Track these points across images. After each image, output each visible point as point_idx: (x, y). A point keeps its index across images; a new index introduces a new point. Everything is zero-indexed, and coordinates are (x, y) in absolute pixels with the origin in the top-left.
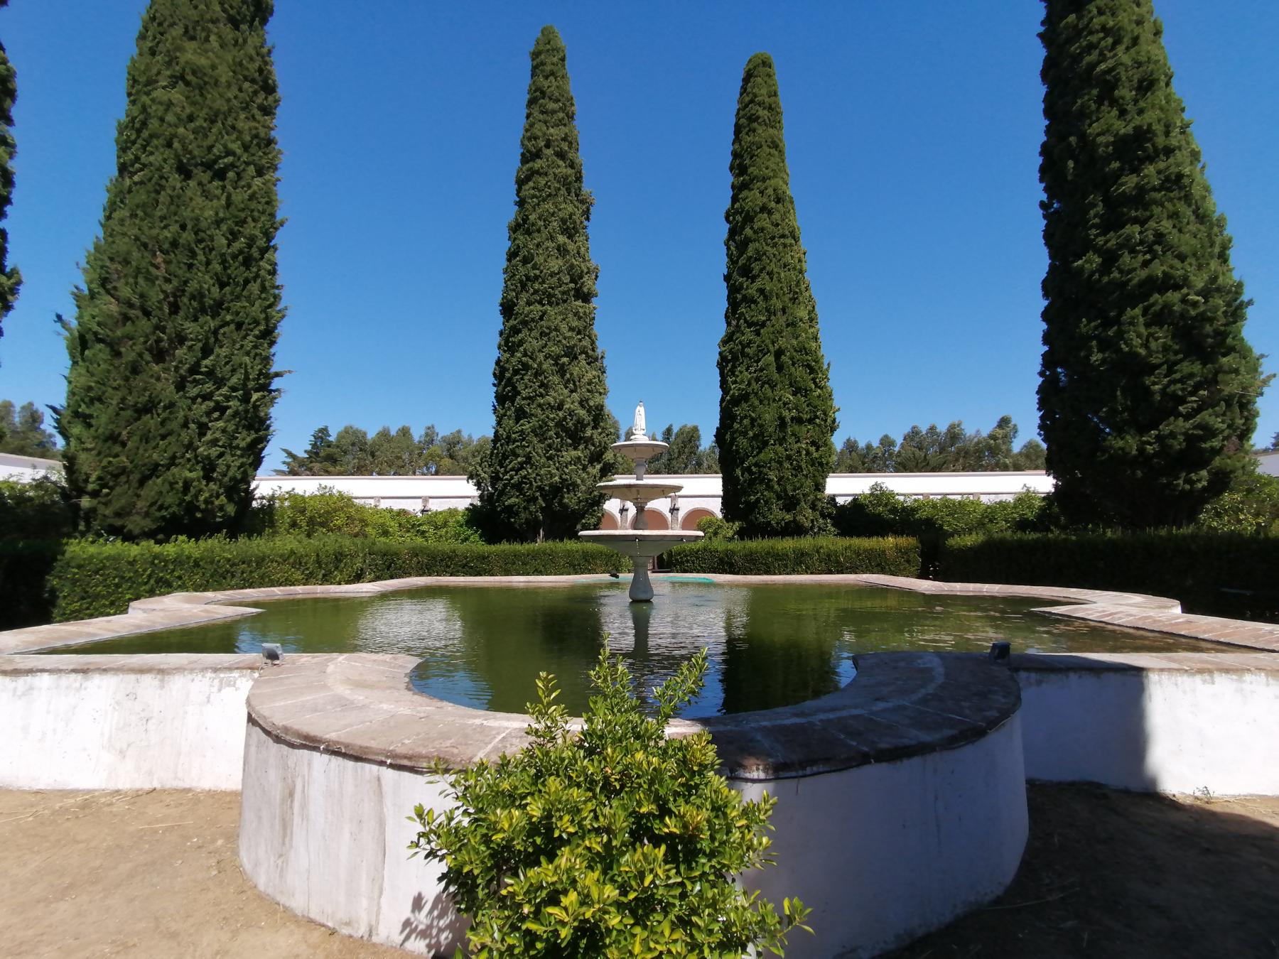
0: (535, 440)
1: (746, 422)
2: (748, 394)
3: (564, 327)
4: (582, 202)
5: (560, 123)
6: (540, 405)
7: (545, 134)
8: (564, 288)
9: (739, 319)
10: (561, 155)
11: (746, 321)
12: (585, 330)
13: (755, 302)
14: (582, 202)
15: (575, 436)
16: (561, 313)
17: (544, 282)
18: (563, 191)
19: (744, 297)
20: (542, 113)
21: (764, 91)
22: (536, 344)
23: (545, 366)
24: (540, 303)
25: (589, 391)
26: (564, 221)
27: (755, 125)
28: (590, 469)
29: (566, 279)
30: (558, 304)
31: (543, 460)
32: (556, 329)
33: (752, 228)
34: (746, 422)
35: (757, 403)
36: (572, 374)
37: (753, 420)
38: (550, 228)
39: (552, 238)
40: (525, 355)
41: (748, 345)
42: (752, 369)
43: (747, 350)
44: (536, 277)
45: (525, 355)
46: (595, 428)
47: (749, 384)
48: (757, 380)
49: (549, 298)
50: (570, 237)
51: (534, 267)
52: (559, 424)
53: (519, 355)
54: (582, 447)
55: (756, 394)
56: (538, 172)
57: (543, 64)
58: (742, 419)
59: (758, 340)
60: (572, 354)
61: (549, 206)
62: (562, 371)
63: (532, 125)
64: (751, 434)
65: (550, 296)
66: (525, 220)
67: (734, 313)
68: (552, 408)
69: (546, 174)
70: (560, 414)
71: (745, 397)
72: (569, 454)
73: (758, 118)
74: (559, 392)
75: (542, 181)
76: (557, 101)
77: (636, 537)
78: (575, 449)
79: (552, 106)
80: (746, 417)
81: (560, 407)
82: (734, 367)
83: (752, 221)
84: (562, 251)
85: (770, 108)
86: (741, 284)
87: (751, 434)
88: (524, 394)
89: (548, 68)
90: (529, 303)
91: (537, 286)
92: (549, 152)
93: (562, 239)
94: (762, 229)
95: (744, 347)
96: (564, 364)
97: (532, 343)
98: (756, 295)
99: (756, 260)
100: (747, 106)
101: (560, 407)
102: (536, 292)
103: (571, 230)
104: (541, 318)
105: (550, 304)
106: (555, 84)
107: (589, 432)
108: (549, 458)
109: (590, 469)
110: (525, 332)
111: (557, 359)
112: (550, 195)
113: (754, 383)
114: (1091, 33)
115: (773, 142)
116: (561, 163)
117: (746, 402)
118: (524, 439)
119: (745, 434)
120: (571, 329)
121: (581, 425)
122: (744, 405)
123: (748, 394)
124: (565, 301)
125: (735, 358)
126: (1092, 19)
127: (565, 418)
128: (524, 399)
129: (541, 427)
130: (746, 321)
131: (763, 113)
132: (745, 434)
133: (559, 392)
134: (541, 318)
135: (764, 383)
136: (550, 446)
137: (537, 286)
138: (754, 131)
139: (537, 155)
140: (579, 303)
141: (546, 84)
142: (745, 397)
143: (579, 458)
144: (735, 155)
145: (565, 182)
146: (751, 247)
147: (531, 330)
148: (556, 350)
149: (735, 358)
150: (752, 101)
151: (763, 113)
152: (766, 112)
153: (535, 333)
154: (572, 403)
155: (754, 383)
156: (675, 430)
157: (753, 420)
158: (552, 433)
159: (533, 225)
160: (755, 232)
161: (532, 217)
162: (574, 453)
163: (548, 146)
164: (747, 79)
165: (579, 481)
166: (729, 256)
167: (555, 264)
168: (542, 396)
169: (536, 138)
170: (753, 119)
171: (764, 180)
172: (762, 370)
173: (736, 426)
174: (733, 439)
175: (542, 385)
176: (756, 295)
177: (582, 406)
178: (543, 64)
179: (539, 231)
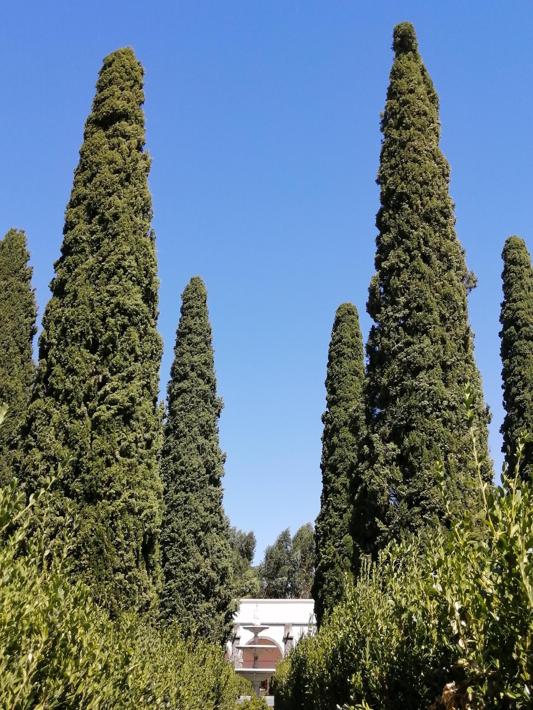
0: (179, 595)
1: (332, 584)
2: (333, 563)
3: (201, 509)
4: (216, 407)
5: (203, 351)
6: (183, 569)
7: (190, 362)
8: (202, 479)
9: (328, 505)
10: (202, 375)
11: (333, 507)
12: (215, 510)
13: (339, 493)
14: (216, 407)
15: (207, 592)
16: (199, 497)
17: (188, 476)
18: (203, 403)
19: (332, 488)
20: (189, 344)
21: (348, 334)
22: (181, 523)
23: (187, 540)
24: (184, 490)
25: (218, 557)
26: (202, 426)
27: (342, 359)
28: (217, 616)
29: (203, 471)
30: (197, 491)
31: (185, 610)
32: (196, 511)
33: (338, 437)
34: (332, 584)
35: (339, 570)
36: (205, 544)
37: (337, 583)
38: (192, 432)
39: (194, 440)
40: (173, 531)
41: (334, 526)
42: (337, 544)
43: (334, 529)
44: (183, 472)
45: (173, 531)
46: (221, 584)
47: (334, 556)
48: (340, 552)
49: (190, 487)
50: (206, 438)
51: (182, 464)
52: (197, 582)
53: (168, 531)
54: (212, 600)
55: (339, 563)
56: (185, 391)
57: (191, 307)
58: (329, 582)
59: (341, 522)
60: (205, 528)
61: (193, 416)
62: (198, 542)
63: (182, 354)
64: (335, 593)
65: (192, 486)
66: (176, 427)
67: (326, 499)
68: (191, 571)
69: (191, 391)
70: (197, 575)
71: (330, 566)
72: (203, 606)
73: (344, 354)
74: (197, 558)
75: (188, 397)
76: (200, 334)
77: (254, 672)
78: (207, 601)
79: (197, 339)
80: (332, 580)
81: (197, 570)
82: (324, 541)
83: (338, 431)
84: (201, 449)
85: (353, 346)
86: (331, 478)
87: (335, 593)
88: (172, 560)
89: (195, 310)
90: (177, 491)
91: (183, 478)
92: (193, 374)
93: (201, 440)
94: (345, 439)
95: (331, 527)
96: (200, 537)
97: (178, 522)
98: (340, 488)
99: (340, 461)
100: (336, 343)
101: (197, 570)
102: (182, 483)
103: (208, 431)
104: (185, 502)
105: (192, 491)
106: (199, 321)
107: (217, 588)
108: (189, 609)
109: (217, 616)
110: (173, 513)
111: (195, 533)
112: (193, 407)
113: (337, 555)
114: (514, 375)
115: (355, 371)
116: (201, 381)
117: (332, 569)
118: (170, 595)
119: (331, 593)
120: (206, 510)
121: (211, 583)
122: (331, 571)
123: (333, 563)
124: (202, 488)
125: (325, 535)
126: (514, 367)
127: (201, 579)
128: (171, 564)
129: (183, 585)
130: (333, 507)
131: (348, 351)
132: (331, 593)
133: (197, 558)
134: (185, 502)
135: (345, 556)
136: (189, 600)
137: (183, 478)
138: (341, 363)
139: (185, 377)
140: (212, 487)
141: (192, 322)
142: (330, 566)
143: (210, 608)
144: (329, 377)
145: (204, 396)
146: (338, 451)
147: (177, 511)
148: (194, 526)
149: (325, 535)
150: (340, 341)
151: (348, 351)
152: (350, 350)
153: (181, 514)
154: (206, 566)
155: (337, 555)
156: (292, 535)
157: (337, 583)
158: (191, 590)
159: (181, 432)
160: (340, 440)
161: (181, 425)
162: (206, 605)
163: (192, 370)
164: (338, 322)
165: (210, 626)
166: (324, 453)
167: (197, 461)
168: (184, 561)
169: (185, 365)
170: (340, 354)
171: (347, 401)
172: (343, 546)
173: (325, 586)
174: (323, 596)
175: (185, 553)
176: (340, 488)
177: (214, 569)
178: (191, 307)
179: (185, 436)
